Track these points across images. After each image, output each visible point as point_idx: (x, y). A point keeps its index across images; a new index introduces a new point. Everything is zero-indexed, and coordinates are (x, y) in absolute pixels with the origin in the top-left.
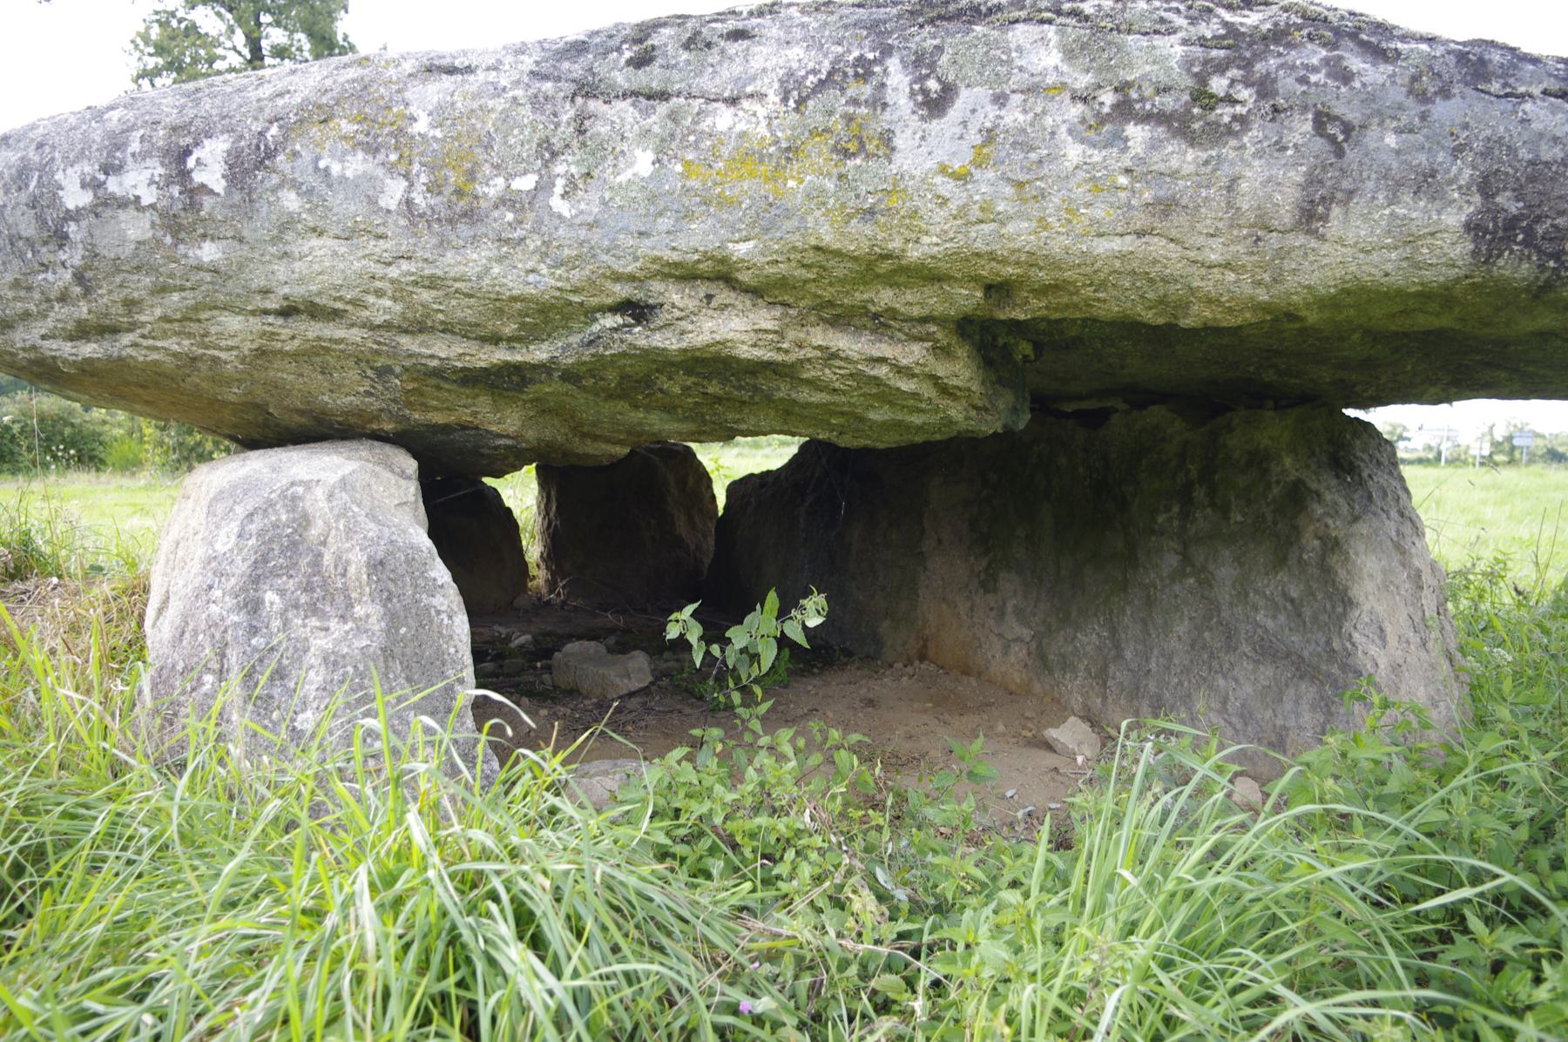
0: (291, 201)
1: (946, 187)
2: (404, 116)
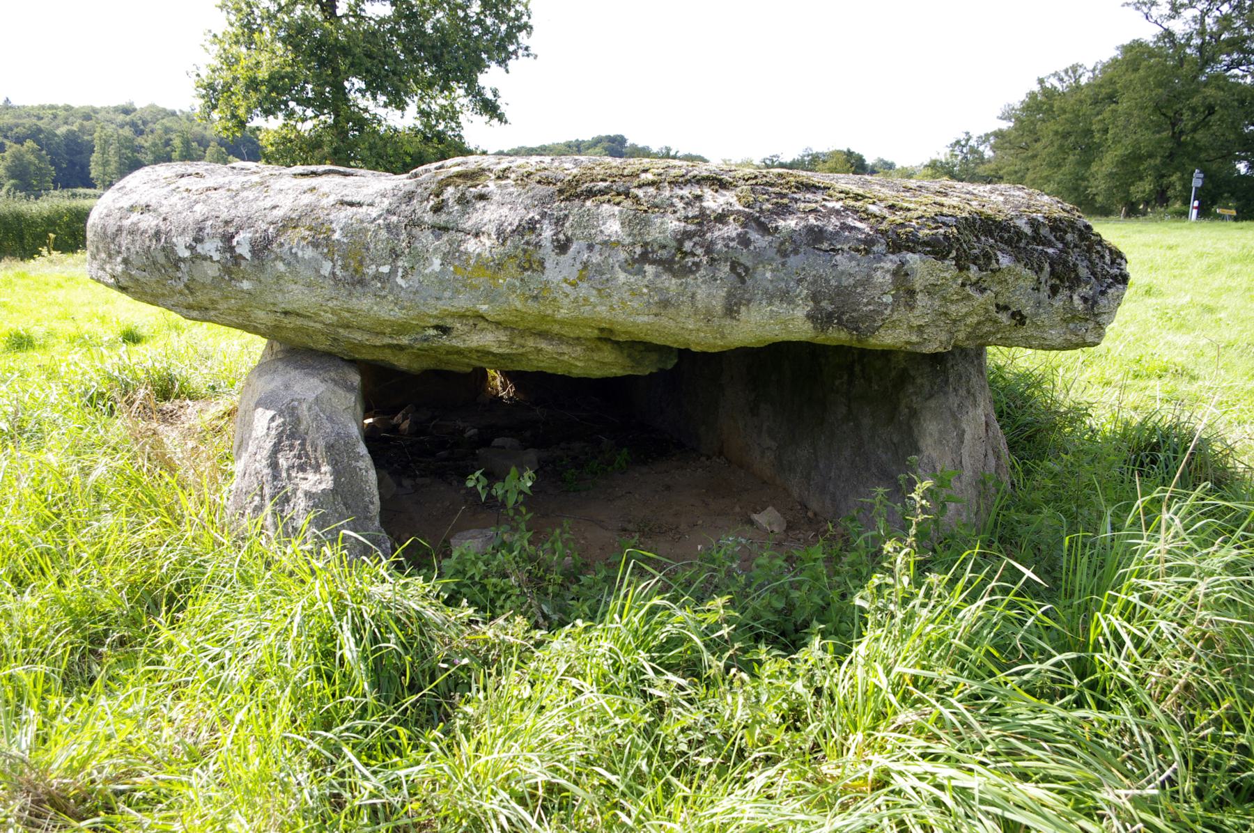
0: (281, 266)
1: (568, 289)
2: (329, 229)
